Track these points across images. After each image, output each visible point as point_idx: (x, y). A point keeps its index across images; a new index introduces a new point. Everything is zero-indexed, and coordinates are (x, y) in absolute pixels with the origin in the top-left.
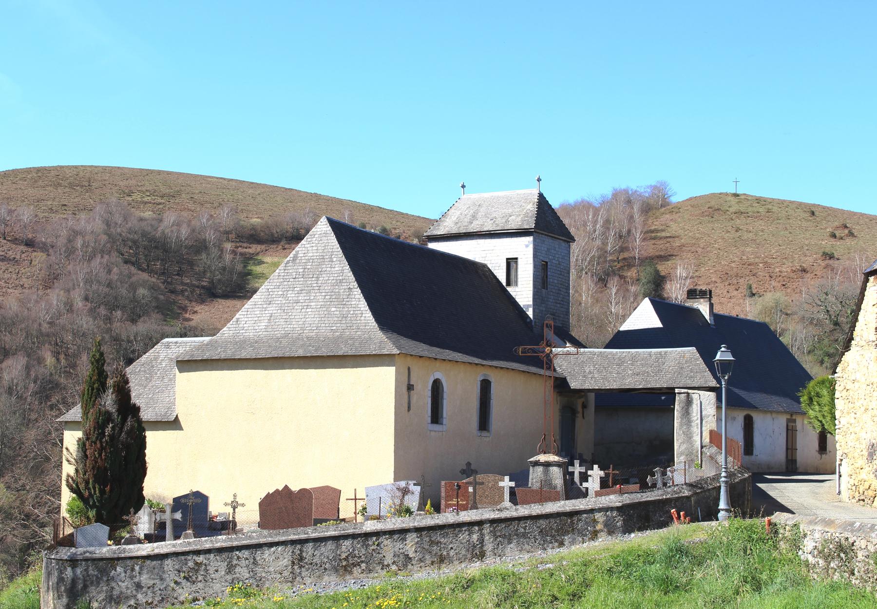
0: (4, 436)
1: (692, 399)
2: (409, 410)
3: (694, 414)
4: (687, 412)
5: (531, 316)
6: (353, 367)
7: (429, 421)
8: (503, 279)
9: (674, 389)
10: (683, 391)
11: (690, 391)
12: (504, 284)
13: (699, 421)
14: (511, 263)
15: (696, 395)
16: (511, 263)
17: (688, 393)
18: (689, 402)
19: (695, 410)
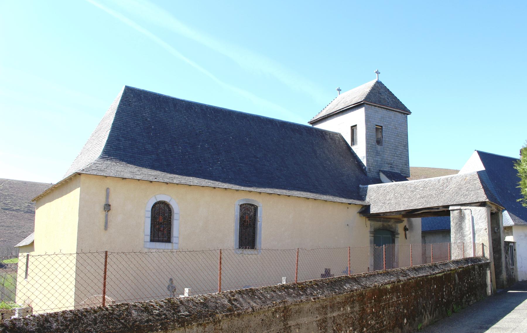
0: (361, 321)
1: (464, 215)
2: (106, 227)
3: (467, 229)
4: (460, 228)
5: (365, 165)
6: (58, 198)
7: (148, 238)
8: (349, 142)
9: (448, 206)
10: (456, 208)
11: (462, 208)
12: (350, 145)
13: (471, 235)
14: (353, 128)
15: (467, 211)
16: (353, 128)
17: (460, 210)
18: (462, 217)
19: (467, 225)
